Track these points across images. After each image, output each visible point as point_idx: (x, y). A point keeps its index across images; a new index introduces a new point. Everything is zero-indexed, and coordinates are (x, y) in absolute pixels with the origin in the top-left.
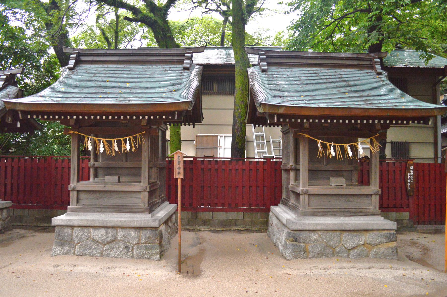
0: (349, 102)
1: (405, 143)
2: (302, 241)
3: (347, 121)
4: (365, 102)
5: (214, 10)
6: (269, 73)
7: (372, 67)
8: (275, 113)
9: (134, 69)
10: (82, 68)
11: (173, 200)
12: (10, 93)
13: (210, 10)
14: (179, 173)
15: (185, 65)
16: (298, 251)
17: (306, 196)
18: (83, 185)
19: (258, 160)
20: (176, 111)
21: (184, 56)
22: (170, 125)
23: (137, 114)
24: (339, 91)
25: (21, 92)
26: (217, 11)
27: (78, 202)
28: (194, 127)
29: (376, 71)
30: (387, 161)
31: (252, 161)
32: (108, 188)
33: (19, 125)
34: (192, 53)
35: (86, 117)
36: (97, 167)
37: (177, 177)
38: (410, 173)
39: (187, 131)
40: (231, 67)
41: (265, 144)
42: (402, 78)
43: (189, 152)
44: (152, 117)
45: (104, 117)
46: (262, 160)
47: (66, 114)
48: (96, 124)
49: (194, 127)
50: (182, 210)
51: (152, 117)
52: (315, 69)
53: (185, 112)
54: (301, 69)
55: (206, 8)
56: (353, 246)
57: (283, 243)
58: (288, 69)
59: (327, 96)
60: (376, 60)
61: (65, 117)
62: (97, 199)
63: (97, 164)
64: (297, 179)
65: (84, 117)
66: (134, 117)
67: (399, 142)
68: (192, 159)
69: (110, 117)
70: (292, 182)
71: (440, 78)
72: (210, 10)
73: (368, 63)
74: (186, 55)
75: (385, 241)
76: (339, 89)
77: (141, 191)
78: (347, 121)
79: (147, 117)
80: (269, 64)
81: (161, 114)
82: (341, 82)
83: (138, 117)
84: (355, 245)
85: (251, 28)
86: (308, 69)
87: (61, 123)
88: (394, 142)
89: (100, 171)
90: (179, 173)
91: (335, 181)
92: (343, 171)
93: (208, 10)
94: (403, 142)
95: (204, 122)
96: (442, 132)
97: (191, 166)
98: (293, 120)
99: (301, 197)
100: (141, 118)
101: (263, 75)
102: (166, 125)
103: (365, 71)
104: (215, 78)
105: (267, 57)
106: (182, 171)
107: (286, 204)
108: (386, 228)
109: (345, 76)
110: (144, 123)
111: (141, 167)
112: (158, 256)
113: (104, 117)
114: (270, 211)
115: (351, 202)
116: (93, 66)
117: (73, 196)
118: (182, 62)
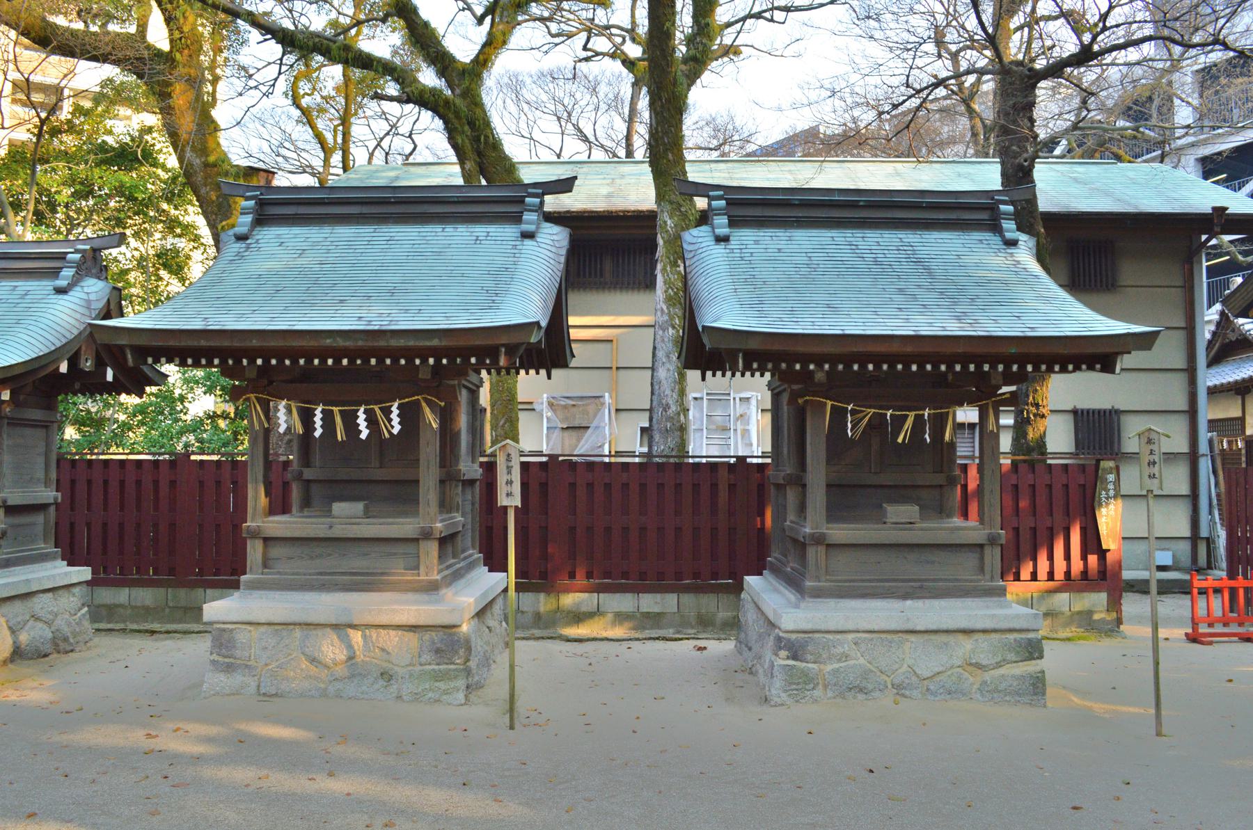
0: (920, 319)
1: (1110, 411)
2: (809, 657)
3: (914, 368)
4: (959, 319)
5: (604, 54)
6: (734, 243)
7: (996, 228)
8: (740, 350)
9: (398, 236)
10: (269, 235)
11: (496, 562)
12: (93, 297)
13: (597, 54)
14: (510, 496)
15: (525, 227)
16: (798, 684)
17: (822, 549)
18: (278, 525)
19: (760, 461)
20: (503, 345)
21: (523, 202)
22: (489, 373)
23: (410, 353)
24: (901, 291)
25: (116, 293)
26: (613, 56)
27: (265, 565)
28: (549, 377)
29: (1002, 236)
30: (1049, 462)
31: (628, 464)
32: (338, 532)
33: (110, 376)
34: (543, 194)
35: (287, 362)
36: (308, 481)
37: (505, 503)
38: (1107, 491)
39: (529, 384)
40: (645, 220)
41: (736, 422)
42: (1086, 250)
43: (537, 438)
44: (444, 361)
45: (330, 362)
46: (637, 460)
47: (238, 354)
48: (307, 376)
49: (549, 377)
50: (520, 588)
51: (444, 361)
52: (848, 233)
53: (524, 347)
54: (814, 233)
55: (585, 48)
56: (937, 670)
57: (766, 666)
58: (781, 233)
59: (868, 305)
60: (1002, 207)
61: (238, 361)
62: (311, 558)
63: (308, 474)
64: (802, 508)
65: (280, 361)
66: (403, 362)
67: (1094, 411)
68: (544, 459)
69: (345, 362)
70: (791, 516)
71: (1204, 237)
72: (597, 54)
73: (984, 216)
74: (527, 199)
75: (1014, 659)
76: (902, 285)
77: (417, 540)
78: (914, 368)
79: (431, 361)
80: (734, 223)
81: (466, 352)
82: (912, 265)
83: (410, 361)
84: (941, 669)
85: (708, 99)
86: (834, 233)
87: (223, 373)
88: (1082, 411)
89: (315, 489)
90: (510, 496)
91: (898, 512)
92: (919, 486)
93: (590, 54)
94: (1105, 411)
95: (573, 363)
96: (1210, 384)
97: (542, 476)
98: (784, 365)
99: (811, 552)
100: (418, 362)
101: (720, 249)
102: (479, 373)
103: (977, 235)
104: (608, 250)
105: (730, 203)
106: (517, 488)
107: (777, 572)
108: (1017, 626)
109: (923, 252)
110: (424, 375)
111: (418, 481)
112: (461, 696)
113: (330, 362)
114: (742, 589)
115: (933, 562)
116: (296, 230)
117: (254, 551)
118: (516, 219)
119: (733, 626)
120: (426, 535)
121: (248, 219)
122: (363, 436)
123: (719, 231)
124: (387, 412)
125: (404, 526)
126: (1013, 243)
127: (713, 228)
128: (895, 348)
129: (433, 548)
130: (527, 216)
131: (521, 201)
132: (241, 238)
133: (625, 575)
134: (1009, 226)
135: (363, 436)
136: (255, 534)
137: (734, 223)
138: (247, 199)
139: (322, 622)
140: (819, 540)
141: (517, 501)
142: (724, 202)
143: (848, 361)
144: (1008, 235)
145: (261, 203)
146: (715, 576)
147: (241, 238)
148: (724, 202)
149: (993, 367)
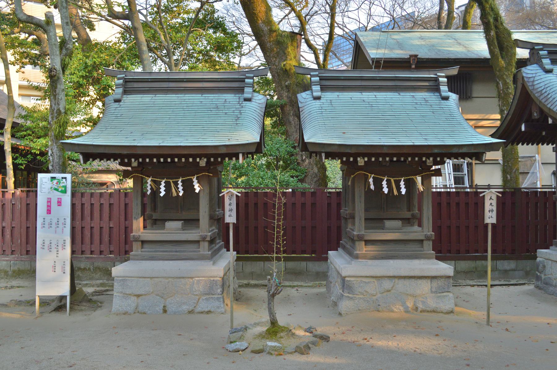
10: (130, 99)
21: (244, 81)
60: (441, 79)
74: (246, 80)
80: (323, 89)
119: (323, 276)
120: (204, 239)
121: (120, 90)
122: (162, 195)
123: (315, 94)
124: (176, 184)
125: (192, 235)
126: (446, 98)
127: (312, 92)
128: (385, 151)
129: (206, 244)
130: (246, 90)
131: (243, 81)
132: (118, 101)
133: (449, 251)
134: (444, 88)
135: (162, 195)
136: (137, 240)
137: (323, 89)
138: (119, 79)
139: (147, 276)
140: (360, 238)
141: (494, 221)
142: (318, 78)
143: (151, 158)
144: (444, 94)
145: (126, 81)
146: (468, 252)
147: (118, 101)
148: (318, 78)
149: (384, 159)
